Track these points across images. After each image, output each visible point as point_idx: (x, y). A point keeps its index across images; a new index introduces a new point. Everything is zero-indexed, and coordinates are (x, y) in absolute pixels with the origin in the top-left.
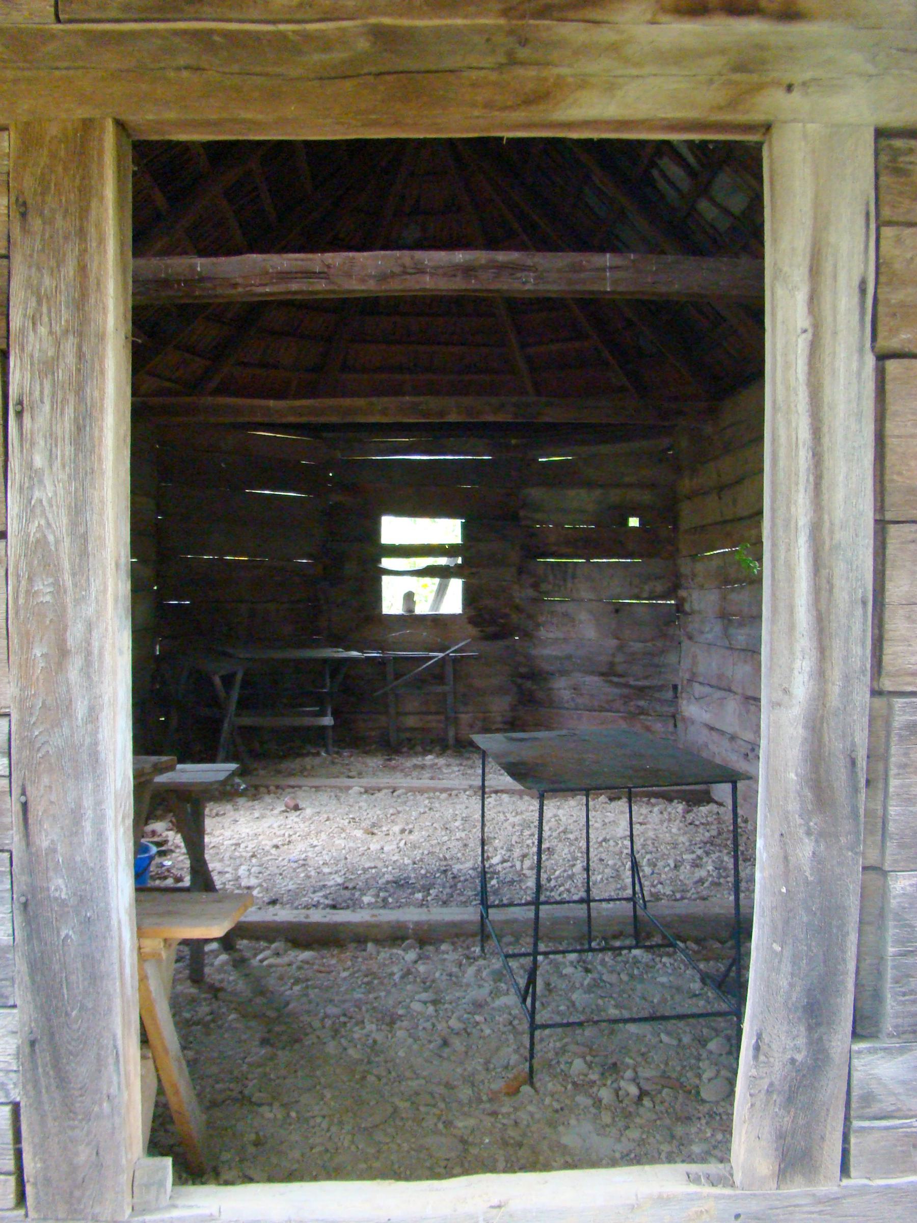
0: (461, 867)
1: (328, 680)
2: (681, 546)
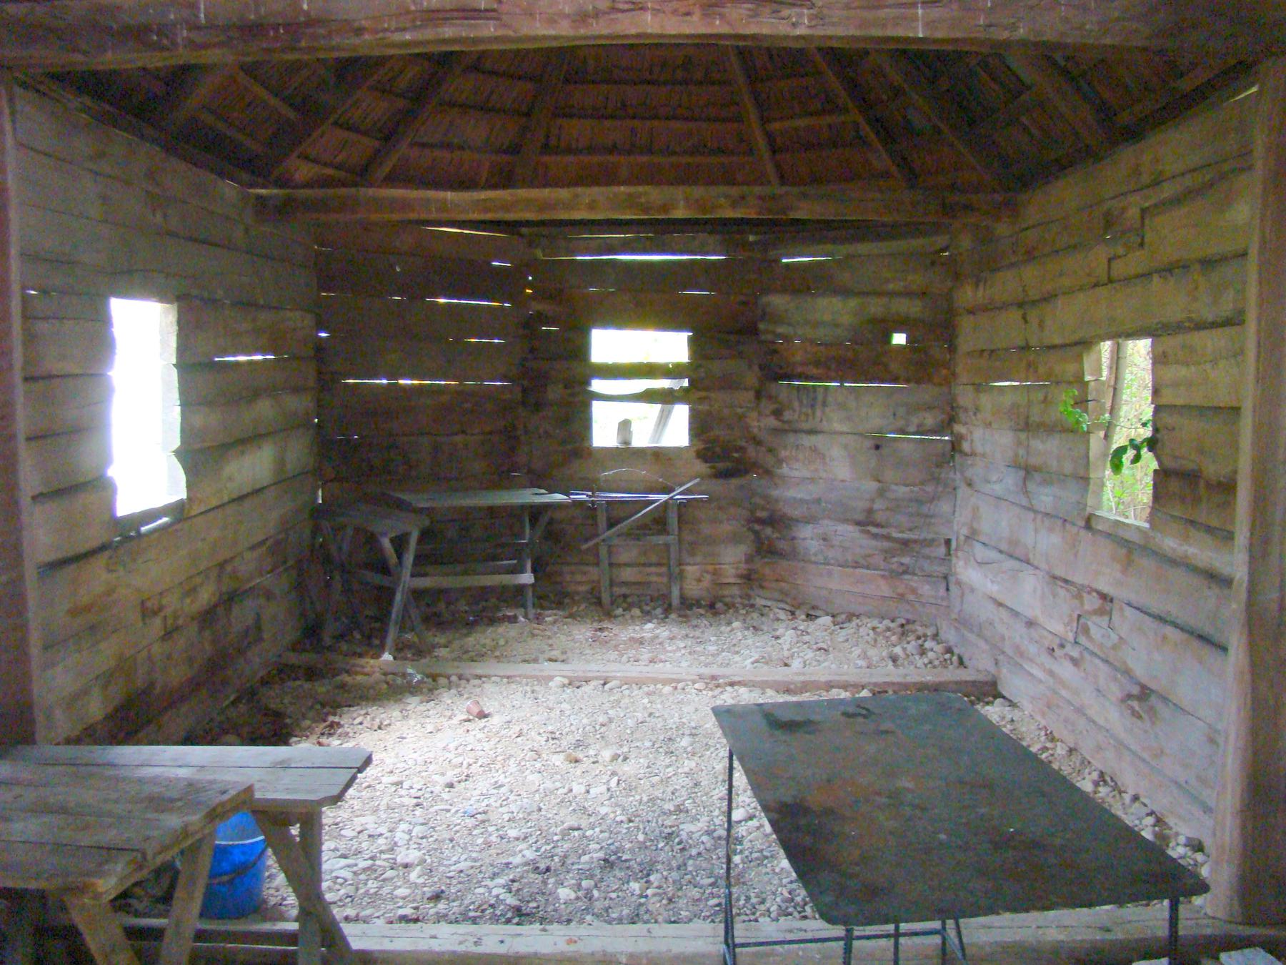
0: (692, 828)
1: (527, 531)
2: (959, 369)
